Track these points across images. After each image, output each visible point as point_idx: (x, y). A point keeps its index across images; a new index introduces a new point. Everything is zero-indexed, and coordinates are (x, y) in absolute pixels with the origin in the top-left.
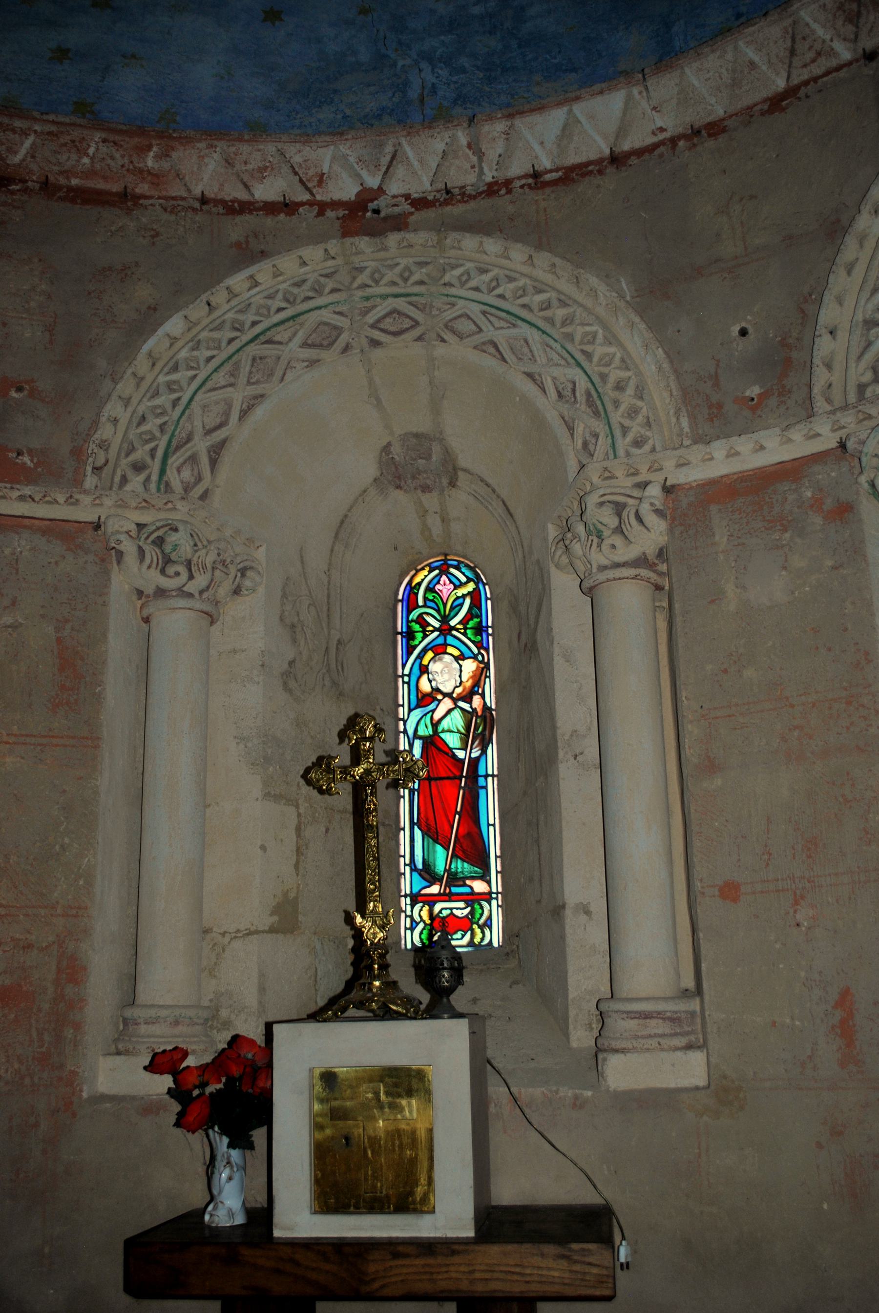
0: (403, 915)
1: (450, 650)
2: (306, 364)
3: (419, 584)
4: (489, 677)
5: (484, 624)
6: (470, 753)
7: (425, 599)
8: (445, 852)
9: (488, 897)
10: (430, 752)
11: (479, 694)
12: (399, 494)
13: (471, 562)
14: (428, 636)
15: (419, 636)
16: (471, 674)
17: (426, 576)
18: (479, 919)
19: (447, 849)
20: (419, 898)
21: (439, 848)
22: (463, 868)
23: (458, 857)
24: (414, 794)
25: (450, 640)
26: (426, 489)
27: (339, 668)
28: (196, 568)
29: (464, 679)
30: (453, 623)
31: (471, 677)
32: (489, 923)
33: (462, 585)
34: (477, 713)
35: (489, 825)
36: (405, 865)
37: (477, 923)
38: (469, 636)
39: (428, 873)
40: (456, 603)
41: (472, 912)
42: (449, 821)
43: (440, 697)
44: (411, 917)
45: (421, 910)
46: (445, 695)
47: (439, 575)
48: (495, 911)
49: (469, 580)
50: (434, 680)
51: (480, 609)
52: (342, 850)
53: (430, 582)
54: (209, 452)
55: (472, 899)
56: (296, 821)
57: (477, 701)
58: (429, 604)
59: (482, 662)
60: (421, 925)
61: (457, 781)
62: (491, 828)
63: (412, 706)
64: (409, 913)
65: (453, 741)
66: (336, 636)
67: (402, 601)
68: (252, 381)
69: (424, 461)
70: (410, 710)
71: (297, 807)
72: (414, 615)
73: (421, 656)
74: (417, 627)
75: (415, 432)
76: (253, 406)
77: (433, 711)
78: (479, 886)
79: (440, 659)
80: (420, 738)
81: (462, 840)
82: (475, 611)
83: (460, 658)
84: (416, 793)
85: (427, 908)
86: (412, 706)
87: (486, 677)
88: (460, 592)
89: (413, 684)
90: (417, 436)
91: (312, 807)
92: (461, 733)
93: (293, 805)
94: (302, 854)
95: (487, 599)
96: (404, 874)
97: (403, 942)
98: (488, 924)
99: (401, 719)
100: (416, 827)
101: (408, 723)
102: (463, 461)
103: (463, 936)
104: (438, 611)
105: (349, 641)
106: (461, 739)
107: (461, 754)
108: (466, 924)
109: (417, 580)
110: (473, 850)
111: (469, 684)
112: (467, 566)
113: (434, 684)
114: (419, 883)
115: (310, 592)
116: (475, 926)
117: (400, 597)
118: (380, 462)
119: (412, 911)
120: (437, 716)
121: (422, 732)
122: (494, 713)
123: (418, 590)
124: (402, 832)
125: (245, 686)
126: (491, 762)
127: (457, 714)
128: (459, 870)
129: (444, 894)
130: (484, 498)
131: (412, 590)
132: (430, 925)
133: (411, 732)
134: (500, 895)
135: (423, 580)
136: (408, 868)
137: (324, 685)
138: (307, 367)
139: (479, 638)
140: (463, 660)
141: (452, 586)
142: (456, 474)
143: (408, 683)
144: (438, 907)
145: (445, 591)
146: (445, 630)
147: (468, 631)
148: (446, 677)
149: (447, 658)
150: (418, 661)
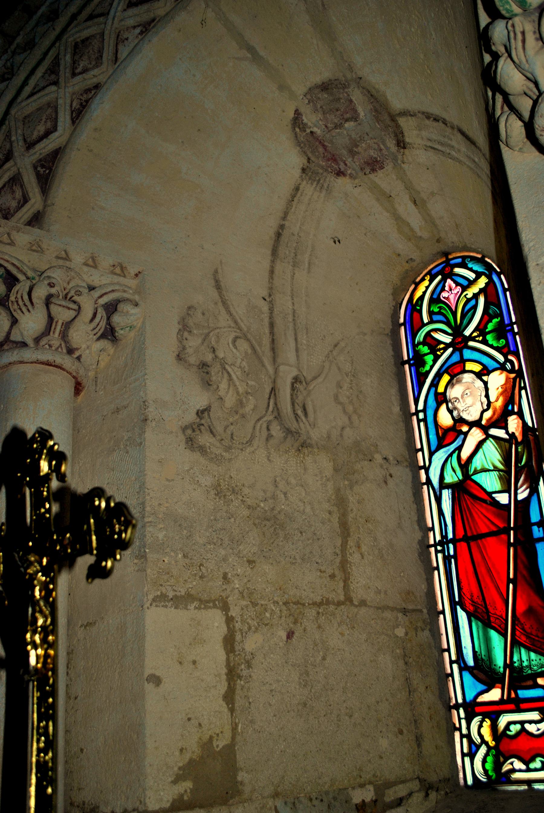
0: (457, 735)
1: (469, 366)
2: (138, 30)
3: (422, 298)
4: (525, 388)
5: (506, 322)
7: (431, 313)
10: (464, 504)
12: (342, 184)
13: (478, 253)
14: (439, 357)
15: (429, 359)
16: (500, 390)
17: (427, 288)
19: (505, 636)
20: (478, 709)
21: (493, 634)
22: (529, 660)
23: (521, 645)
24: (450, 563)
25: (467, 354)
26: (374, 165)
27: (300, 412)
28: (16, 306)
29: (492, 399)
30: (467, 333)
31: (501, 394)
33: (471, 283)
34: (516, 438)
36: (451, 662)
38: (490, 342)
39: (484, 672)
41: (497, 766)
42: (501, 594)
43: (465, 429)
44: (469, 736)
45: (480, 726)
46: (472, 425)
49: (479, 275)
50: (455, 408)
51: (499, 307)
52: (324, 659)
54: (35, 167)
56: (224, 629)
57: (513, 423)
58: (435, 318)
60: (483, 750)
61: (504, 537)
64: (465, 731)
65: (490, 482)
66: (288, 374)
67: (404, 324)
68: (78, 71)
69: (352, 124)
70: (431, 454)
71: (225, 608)
72: (421, 336)
73: (435, 384)
74: (425, 349)
75: (320, 83)
76: (87, 101)
77: (460, 449)
79: (459, 381)
80: (448, 486)
81: (522, 620)
82: (493, 309)
83: (486, 371)
84: (453, 560)
85: (487, 723)
87: (521, 389)
88: (470, 293)
89: (430, 419)
90: (325, 87)
91: (254, 604)
93: (215, 606)
94: (240, 677)
95: (505, 290)
96: (452, 675)
97: (461, 775)
99: (421, 468)
100: (458, 607)
102: (397, 103)
104: (448, 323)
105: (315, 378)
106: (500, 478)
107: (503, 499)
109: (418, 294)
111: (499, 404)
112: (473, 259)
113: (455, 413)
114: (472, 687)
115: (236, 322)
117: (402, 320)
118: (299, 143)
119: (468, 728)
120: (465, 454)
121: (450, 478)
124: (442, 616)
125: (127, 452)
127: (490, 445)
128: (525, 664)
129: (510, 700)
130: (442, 144)
131: (414, 308)
132: (496, 748)
133: (435, 481)
135: (424, 293)
136: (455, 666)
137: (269, 437)
138: (141, 33)
139: (503, 342)
140: (488, 374)
141: (459, 289)
142: (398, 126)
145: (452, 297)
146: (460, 342)
147: (489, 338)
149: (467, 378)
150: (433, 390)
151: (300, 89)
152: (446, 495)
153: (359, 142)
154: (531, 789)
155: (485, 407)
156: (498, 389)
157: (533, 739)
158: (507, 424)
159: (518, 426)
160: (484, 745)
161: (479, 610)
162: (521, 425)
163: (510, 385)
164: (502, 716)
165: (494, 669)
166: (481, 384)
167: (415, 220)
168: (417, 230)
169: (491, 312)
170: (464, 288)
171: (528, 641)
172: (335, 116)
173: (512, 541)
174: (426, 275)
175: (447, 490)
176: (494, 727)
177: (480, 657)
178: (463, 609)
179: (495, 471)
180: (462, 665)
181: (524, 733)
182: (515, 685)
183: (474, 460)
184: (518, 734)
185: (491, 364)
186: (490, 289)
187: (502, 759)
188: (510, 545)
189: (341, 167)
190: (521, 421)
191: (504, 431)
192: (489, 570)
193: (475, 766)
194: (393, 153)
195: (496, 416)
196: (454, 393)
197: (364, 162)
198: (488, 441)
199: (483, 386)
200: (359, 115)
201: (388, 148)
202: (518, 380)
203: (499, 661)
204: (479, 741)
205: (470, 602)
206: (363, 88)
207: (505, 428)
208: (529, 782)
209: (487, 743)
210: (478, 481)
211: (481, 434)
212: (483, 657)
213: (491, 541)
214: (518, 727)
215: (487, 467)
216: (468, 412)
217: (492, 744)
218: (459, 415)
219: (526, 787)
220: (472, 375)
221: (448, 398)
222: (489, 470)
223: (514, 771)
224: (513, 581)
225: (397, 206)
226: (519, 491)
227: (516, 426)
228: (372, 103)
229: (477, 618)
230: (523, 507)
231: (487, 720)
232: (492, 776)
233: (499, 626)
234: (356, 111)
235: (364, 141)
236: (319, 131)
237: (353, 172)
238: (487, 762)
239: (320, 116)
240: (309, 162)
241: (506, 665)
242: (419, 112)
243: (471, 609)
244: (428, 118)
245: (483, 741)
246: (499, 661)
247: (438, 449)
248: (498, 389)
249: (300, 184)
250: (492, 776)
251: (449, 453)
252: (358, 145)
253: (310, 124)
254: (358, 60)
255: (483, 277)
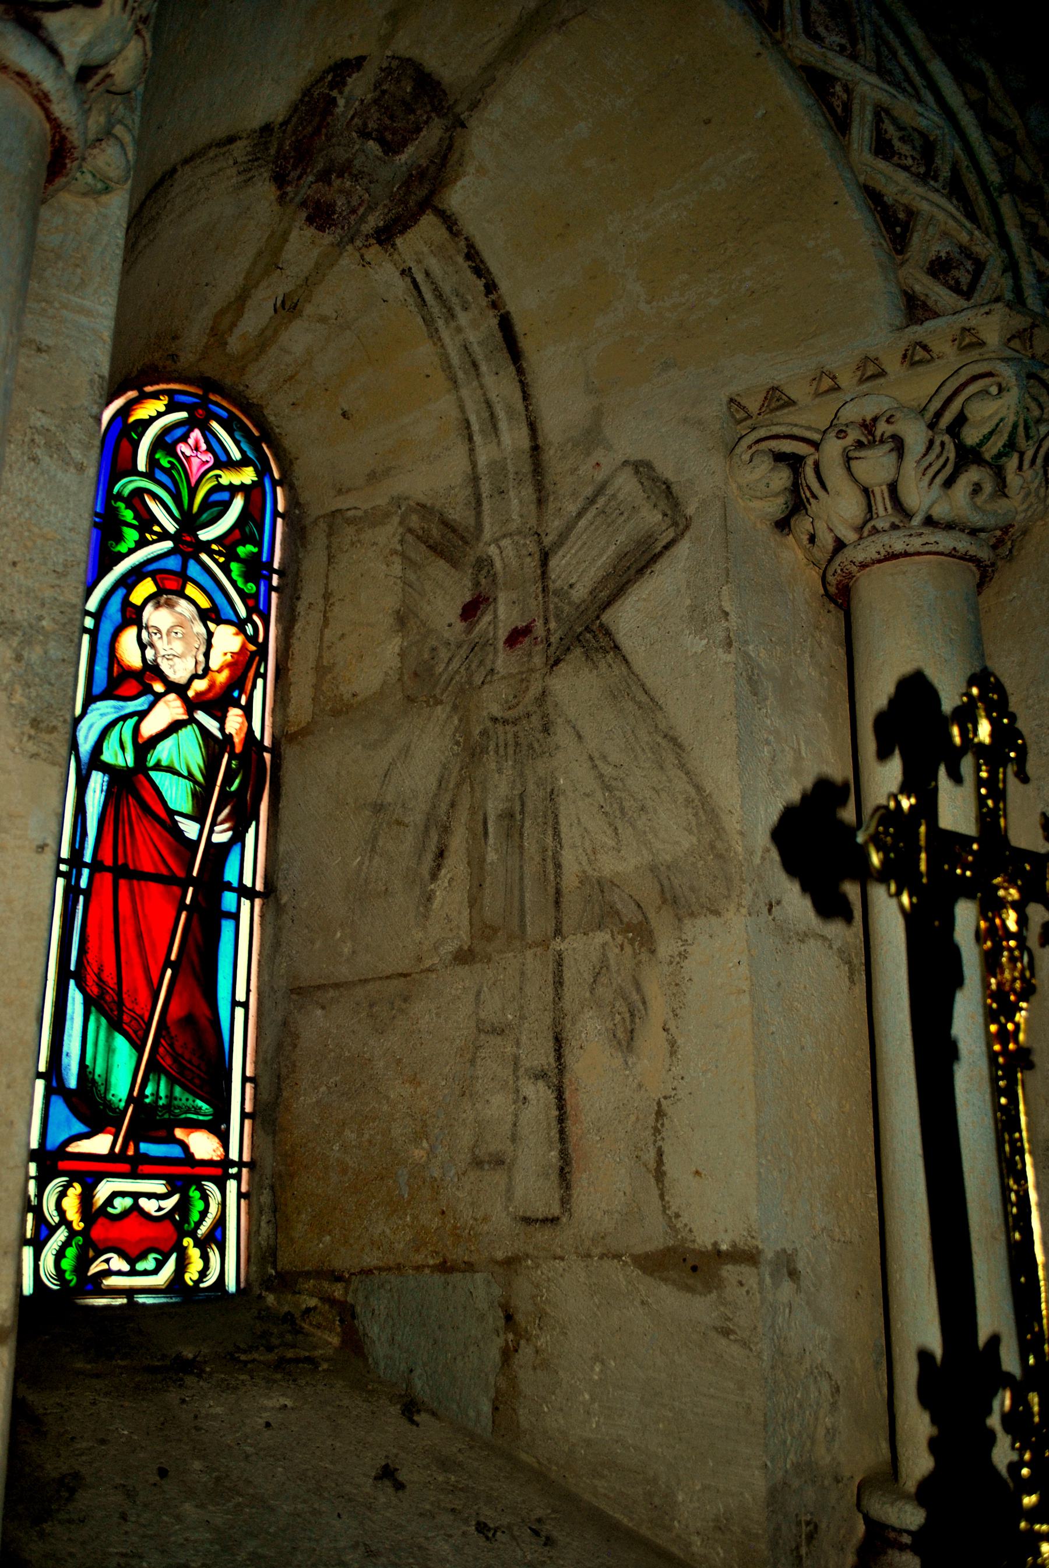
4: (264, 677)
6: (211, 831)
7: (152, 462)
8: (134, 1054)
9: (220, 1171)
11: (240, 706)
15: (131, 536)
16: (229, 658)
17: (160, 415)
18: (198, 1224)
20: (62, 1165)
21: (121, 1043)
22: (170, 1096)
25: (193, 570)
29: (214, 665)
30: (206, 535)
31: (229, 665)
32: (218, 1234)
34: (233, 744)
35: (235, 1003)
37: (193, 1234)
38: (235, 575)
40: (216, 497)
41: (83, 1263)
42: (149, 980)
44: (38, 1211)
45: (62, 1195)
47: (189, 425)
48: (227, 1204)
50: (152, 646)
53: (167, 430)
55: (186, 1175)
57: (234, 720)
59: (252, 639)
60: (61, 1235)
61: (176, 890)
62: (239, 1012)
63: (97, 690)
65: (177, 794)
70: (90, 699)
73: (130, 580)
77: (142, 715)
78: (203, 1145)
79: (170, 605)
81: (174, 1031)
83: (209, 616)
84: (81, 898)
85: (76, 1190)
86: (97, 690)
87: (258, 675)
92: (195, 782)
95: (275, 514)
98: (216, 1237)
100: (72, 982)
101: (84, 725)
103: (160, 1265)
104: (177, 498)
106: (194, 794)
107: (190, 829)
108: (171, 1234)
109: (142, 413)
110: (192, 1057)
111: (222, 678)
113: (150, 654)
116: (188, 1241)
118: (307, 92)
122: (267, 756)
123: (141, 436)
125: (34, 459)
126: (248, 865)
127: (189, 736)
130: (439, 296)
134: (245, 1171)
135: (152, 420)
143: (94, 634)
144: (104, 1190)
145: (195, 462)
146: (187, 545)
147: (234, 566)
148: (178, 647)
150: (121, 592)
151: (403, 45)
152: (98, 781)
153: (350, 174)
154: (131, 1303)
155: (200, 672)
156: (226, 654)
157: (150, 1223)
158: (226, 717)
159: (240, 729)
160: (63, 1227)
161: (107, 998)
162: (245, 729)
163: (243, 660)
164: (105, 1181)
165: (110, 1101)
166: (203, 631)
167: (254, 320)
168: (238, 332)
169: (247, 529)
170: (218, 464)
171: (174, 1067)
172: (378, 119)
173: (188, 901)
174: (163, 392)
175: (100, 774)
176: (86, 1199)
177: (91, 1076)
178: (79, 986)
179: (190, 780)
180: (54, 1084)
181: (135, 1214)
182: (135, 1135)
183: (160, 746)
184: (126, 1213)
185: (227, 612)
186: (256, 493)
187: (91, 1253)
188: (182, 906)
189: (292, 174)
190: (246, 724)
191: (217, 725)
192: (139, 936)
193: (41, 1263)
194: (358, 231)
195: (211, 694)
196: (155, 617)
197: (319, 200)
198: (189, 727)
199: (206, 636)
200: (398, 152)
201: (363, 219)
202: (257, 658)
203: (120, 1089)
204: (57, 1219)
205: (96, 979)
206: (451, 138)
207: (222, 720)
208: (130, 1292)
209: (69, 1225)
210: (157, 782)
211: (181, 710)
212: (96, 1077)
213: (154, 889)
214: (128, 1202)
215: (177, 767)
216: (170, 662)
217: (78, 1226)
218: (155, 660)
219: (125, 1301)
220: (192, 608)
221: (144, 621)
222: (180, 775)
223: (109, 1273)
224: (175, 966)
225: (264, 284)
226: (217, 828)
227: (238, 726)
228: (432, 162)
229: (102, 1011)
230: (218, 854)
231: (76, 1185)
232: (71, 1281)
233: (135, 1032)
234: (405, 146)
235: (357, 180)
236: (342, 109)
237: (291, 195)
238: (65, 1256)
239: (369, 96)
240: (281, 125)
241: (130, 1098)
242: (467, 239)
243: (94, 991)
244: (468, 257)
245: (64, 1221)
246: (120, 1089)
247: (105, 696)
248: (226, 654)
249: (240, 139)
250: (71, 1281)
251: (123, 713)
252: (343, 177)
253: (347, 90)
254: (495, 110)
255: (251, 469)
